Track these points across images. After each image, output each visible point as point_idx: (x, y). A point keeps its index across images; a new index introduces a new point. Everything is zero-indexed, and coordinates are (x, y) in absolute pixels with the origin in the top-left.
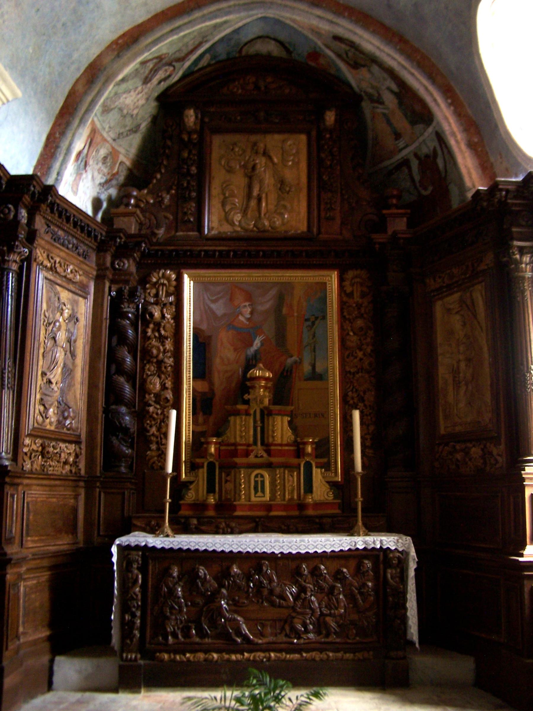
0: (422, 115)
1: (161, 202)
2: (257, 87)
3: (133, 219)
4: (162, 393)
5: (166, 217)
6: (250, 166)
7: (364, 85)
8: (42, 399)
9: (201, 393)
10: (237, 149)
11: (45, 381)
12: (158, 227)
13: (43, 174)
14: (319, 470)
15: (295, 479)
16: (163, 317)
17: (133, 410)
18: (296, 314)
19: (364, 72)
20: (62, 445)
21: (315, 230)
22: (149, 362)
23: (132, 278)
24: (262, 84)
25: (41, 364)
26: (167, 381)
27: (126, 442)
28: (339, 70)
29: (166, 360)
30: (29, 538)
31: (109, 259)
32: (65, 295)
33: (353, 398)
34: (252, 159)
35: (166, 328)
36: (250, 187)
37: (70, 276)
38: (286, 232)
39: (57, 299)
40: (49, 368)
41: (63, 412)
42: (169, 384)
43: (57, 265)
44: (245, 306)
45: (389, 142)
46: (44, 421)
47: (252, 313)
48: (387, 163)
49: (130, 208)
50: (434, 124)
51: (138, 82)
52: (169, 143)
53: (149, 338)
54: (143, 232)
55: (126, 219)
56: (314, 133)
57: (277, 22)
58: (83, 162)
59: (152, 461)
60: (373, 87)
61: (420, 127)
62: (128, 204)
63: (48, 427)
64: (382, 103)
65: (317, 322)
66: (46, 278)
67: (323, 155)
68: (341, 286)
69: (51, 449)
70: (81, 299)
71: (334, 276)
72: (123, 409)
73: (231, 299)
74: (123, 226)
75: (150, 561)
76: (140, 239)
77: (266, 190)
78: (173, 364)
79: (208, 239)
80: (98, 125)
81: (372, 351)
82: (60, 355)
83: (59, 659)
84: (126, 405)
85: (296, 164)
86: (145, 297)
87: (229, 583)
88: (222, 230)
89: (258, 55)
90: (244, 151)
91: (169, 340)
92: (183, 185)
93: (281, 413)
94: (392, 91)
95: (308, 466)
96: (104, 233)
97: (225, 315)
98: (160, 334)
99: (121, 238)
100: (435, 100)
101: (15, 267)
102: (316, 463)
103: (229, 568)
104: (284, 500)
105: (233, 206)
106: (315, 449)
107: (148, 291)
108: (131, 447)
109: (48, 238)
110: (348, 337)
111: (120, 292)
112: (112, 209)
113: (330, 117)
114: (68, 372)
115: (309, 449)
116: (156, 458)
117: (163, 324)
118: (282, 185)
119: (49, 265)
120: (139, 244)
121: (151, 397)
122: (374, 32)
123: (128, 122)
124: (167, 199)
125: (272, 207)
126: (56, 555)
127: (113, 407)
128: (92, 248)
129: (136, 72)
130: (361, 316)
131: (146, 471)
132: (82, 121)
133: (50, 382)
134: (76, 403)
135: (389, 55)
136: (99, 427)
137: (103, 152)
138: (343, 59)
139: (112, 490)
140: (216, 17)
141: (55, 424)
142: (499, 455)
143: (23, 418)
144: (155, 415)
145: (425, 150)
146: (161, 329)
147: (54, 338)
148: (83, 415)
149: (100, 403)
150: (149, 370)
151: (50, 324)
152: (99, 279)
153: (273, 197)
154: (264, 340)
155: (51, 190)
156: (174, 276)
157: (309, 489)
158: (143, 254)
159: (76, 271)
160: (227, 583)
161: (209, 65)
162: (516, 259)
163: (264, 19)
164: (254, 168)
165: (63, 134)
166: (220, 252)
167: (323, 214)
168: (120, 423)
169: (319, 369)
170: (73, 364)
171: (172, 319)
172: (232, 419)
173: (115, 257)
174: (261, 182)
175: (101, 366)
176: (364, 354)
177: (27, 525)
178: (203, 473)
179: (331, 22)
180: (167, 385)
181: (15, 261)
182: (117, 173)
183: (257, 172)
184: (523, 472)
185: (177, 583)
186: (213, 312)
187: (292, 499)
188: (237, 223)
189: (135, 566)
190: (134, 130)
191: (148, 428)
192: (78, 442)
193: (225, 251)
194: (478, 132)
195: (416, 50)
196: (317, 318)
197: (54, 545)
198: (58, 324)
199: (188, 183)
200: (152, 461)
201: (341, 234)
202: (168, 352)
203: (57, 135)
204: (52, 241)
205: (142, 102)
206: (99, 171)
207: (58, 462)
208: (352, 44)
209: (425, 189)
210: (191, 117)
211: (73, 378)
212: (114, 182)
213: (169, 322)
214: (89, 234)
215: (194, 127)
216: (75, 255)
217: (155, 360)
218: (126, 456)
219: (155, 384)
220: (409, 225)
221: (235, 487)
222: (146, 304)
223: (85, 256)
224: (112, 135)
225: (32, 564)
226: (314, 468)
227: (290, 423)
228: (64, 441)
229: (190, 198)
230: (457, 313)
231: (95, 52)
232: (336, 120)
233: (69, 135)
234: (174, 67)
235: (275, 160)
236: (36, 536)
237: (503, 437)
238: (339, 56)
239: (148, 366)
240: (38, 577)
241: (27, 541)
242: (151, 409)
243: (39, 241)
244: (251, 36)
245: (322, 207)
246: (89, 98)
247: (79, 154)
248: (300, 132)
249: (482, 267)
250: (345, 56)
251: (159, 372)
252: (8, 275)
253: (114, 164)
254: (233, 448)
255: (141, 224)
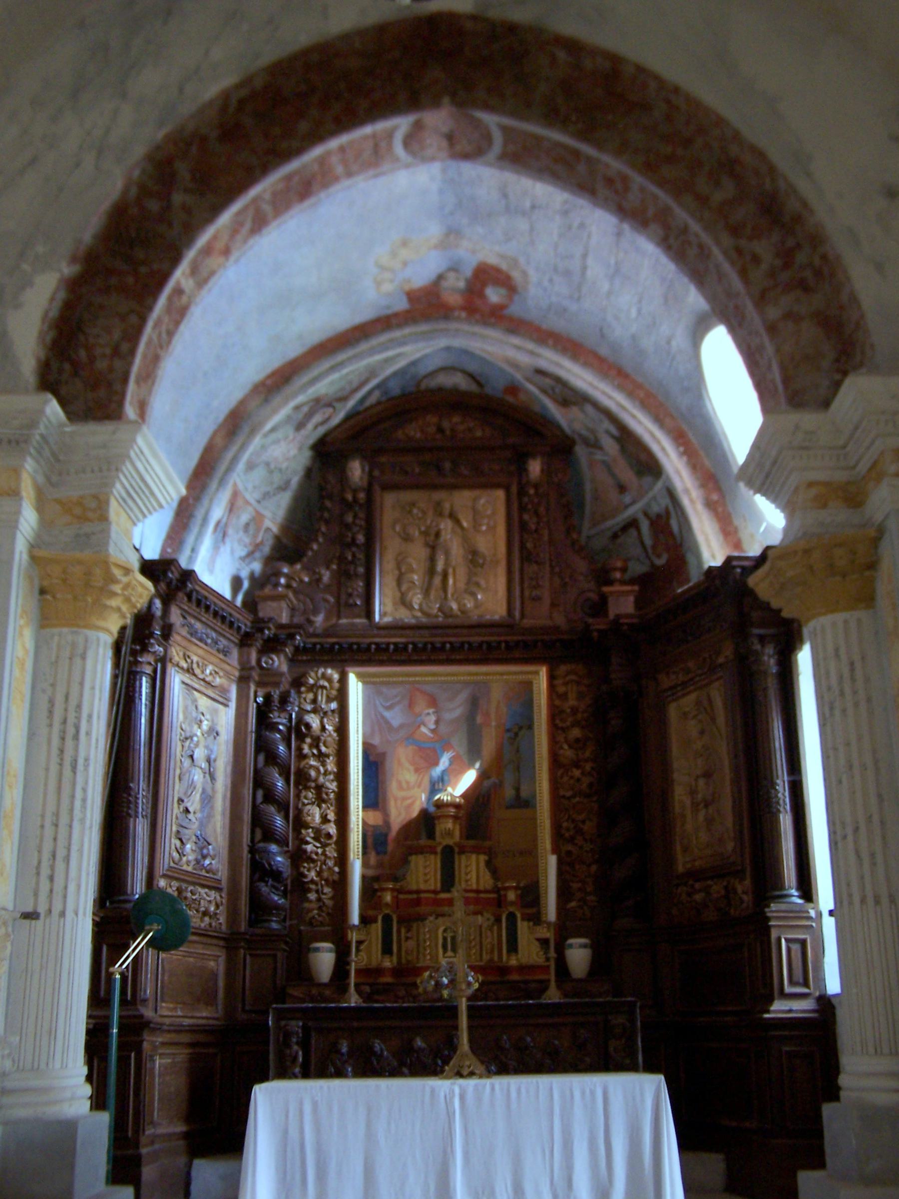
0: (649, 467)
1: (319, 580)
2: (440, 430)
3: (284, 605)
4: (324, 827)
5: (326, 601)
6: (433, 532)
7: (577, 426)
8: (178, 832)
9: (374, 826)
10: (415, 511)
11: (181, 810)
12: (316, 612)
13: (174, 551)
14: (525, 923)
15: (495, 935)
16: (323, 728)
17: (286, 849)
18: (493, 724)
19: (575, 411)
20: (203, 891)
21: (517, 614)
22: (307, 788)
23: (283, 679)
24: (446, 424)
25: (178, 790)
26: (328, 811)
27: (277, 889)
28: (544, 407)
29: (328, 784)
30: (164, 1005)
31: (254, 656)
32: (204, 703)
33: (568, 829)
34: (434, 524)
35: (328, 744)
36: (432, 560)
37: (209, 679)
38: (481, 616)
39: (194, 708)
40: (185, 794)
41: (202, 849)
42: (331, 816)
43: (195, 666)
44: (428, 714)
45: (613, 495)
46: (181, 859)
47: (437, 722)
48: (610, 523)
49: (280, 589)
50: (664, 477)
51: (290, 431)
52: (328, 503)
53: (305, 757)
54: (296, 620)
55: (274, 604)
56: (514, 489)
57: (466, 352)
58: (222, 531)
59: (310, 915)
60: (588, 429)
61: (648, 479)
62: (277, 584)
63: (185, 867)
64: (600, 448)
65: (521, 733)
66: (183, 683)
67: (526, 517)
68: (551, 687)
69: (189, 895)
70: (221, 707)
71: (543, 671)
72: (274, 848)
73: (411, 705)
74: (272, 615)
75: (313, 1034)
76: (293, 631)
77: (454, 563)
78: (336, 790)
79: (380, 628)
80: (241, 487)
81: (592, 768)
82: (198, 777)
83: (197, 1163)
84: (278, 842)
85: (492, 529)
86: (300, 703)
87: (411, 1061)
88: (398, 616)
89: (440, 389)
90: (424, 513)
91: (331, 758)
92: (346, 558)
93: (477, 850)
94: (613, 437)
95: (512, 917)
96: (249, 624)
97: (402, 726)
98: (319, 751)
99: (269, 629)
100: (663, 449)
101: (148, 670)
102: (522, 915)
103: (411, 1041)
104: (481, 960)
105: (411, 585)
106: (521, 897)
107: (304, 695)
108: (285, 894)
109: (184, 632)
110: (561, 752)
111: (268, 698)
112: (257, 591)
113: (535, 468)
114: (207, 799)
115: (511, 896)
116: (316, 912)
117: (322, 738)
118: (474, 558)
119: (185, 665)
120: (292, 637)
121: (308, 833)
122: (586, 365)
123: (277, 479)
124: (326, 576)
125: (461, 585)
126: (193, 1030)
127: (261, 845)
128: (233, 642)
129: (289, 418)
130: (575, 724)
131: (302, 928)
132: (222, 482)
133: (187, 811)
134: (216, 841)
135: (604, 393)
136: (244, 870)
137: (245, 518)
138: (550, 396)
139: (258, 952)
140: (387, 349)
141: (193, 863)
142: (744, 893)
143: (158, 855)
144: (314, 857)
145: (655, 509)
146: (321, 744)
147: (192, 757)
148: (224, 853)
149: (245, 840)
150: (306, 798)
151: (187, 739)
152: (243, 680)
153: (462, 572)
154: (453, 757)
155: (189, 575)
156: (336, 676)
157: (513, 947)
158: (297, 649)
159: (216, 673)
160: (409, 1061)
161: (379, 403)
162: (756, 651)
163: (448, 349)
164: (438, 535)
165: (198, 499)
166: (395, 644)
167: (527, 593)
168: (270, 865)
169: (524, 794)
170: (213, 789)
171: (335, 731)
172: (413, 858)
173: (262, 652)
174: (447, 554)
175: (246, 792)
176: (583, 773)
177: (162, 987)
178: (377, 928)
179: (532, 353)
180: (329, 817)
181: (150, 664)
182: (262, 543)
183: (442, 539)
184: (766, 910)
185: (346, 1062)
186: (387, 722)
187: (491, 960)
188: (416, 607)
189: (294, 1040)
190: (283, 488)
191: (306, 873)
192: (218, 889)
193: (402, 643)
194: (718, 489)
195: (639, 386)
196: (521, 728)
197: (192, 1017)
198: (195, 739)
199: (354, 556)
200: (310, 915)
201: (551, 618)
202: (330, 773)
203: (191, 501)
204: (189, 636)
205: (294, 452)
206: (240, 541)
207: (197, 911)
208: (558, 380)
209: (659, 556)
210: (356, 470)
211: (212, 808)
212: (257, 555)
213: (330, 735)
214: (231, 625)
215: (360, 484)
216: (215, 652)
217: (313, 785)
218: (277, 907)
219: (313, 816)
220: (638, 604)
221: (418, 945)
222: (302, 712)
223: (225, 652)
224: (257, 495)
225: (167, 1038)
226: (519, 923)
227: (488, 864)
228: (203, 886)
229: (356, 575)
230: (695, 717)
231: (238, 395)
232: (542, 471)
233: (205, 502)
234: (334, 408)
235: (465, 524)
236: (172, 1003)
237: (748, 869)
238: (544, 391)
239: (303, 793)
240: (174, 1054)
241: (162, 1007)
242: (309, 848)
243: (175, 637)
244: (431, 368)
245: (526, 585)
246: (229, 455)
247: (218, 524)
248: (497, 486)
249: (721, 660)
250: (550, 392)
251: (320, 800)
252: (141, 679)
253: (258, 530)
254: (415, 896)
255: (293, 609)
